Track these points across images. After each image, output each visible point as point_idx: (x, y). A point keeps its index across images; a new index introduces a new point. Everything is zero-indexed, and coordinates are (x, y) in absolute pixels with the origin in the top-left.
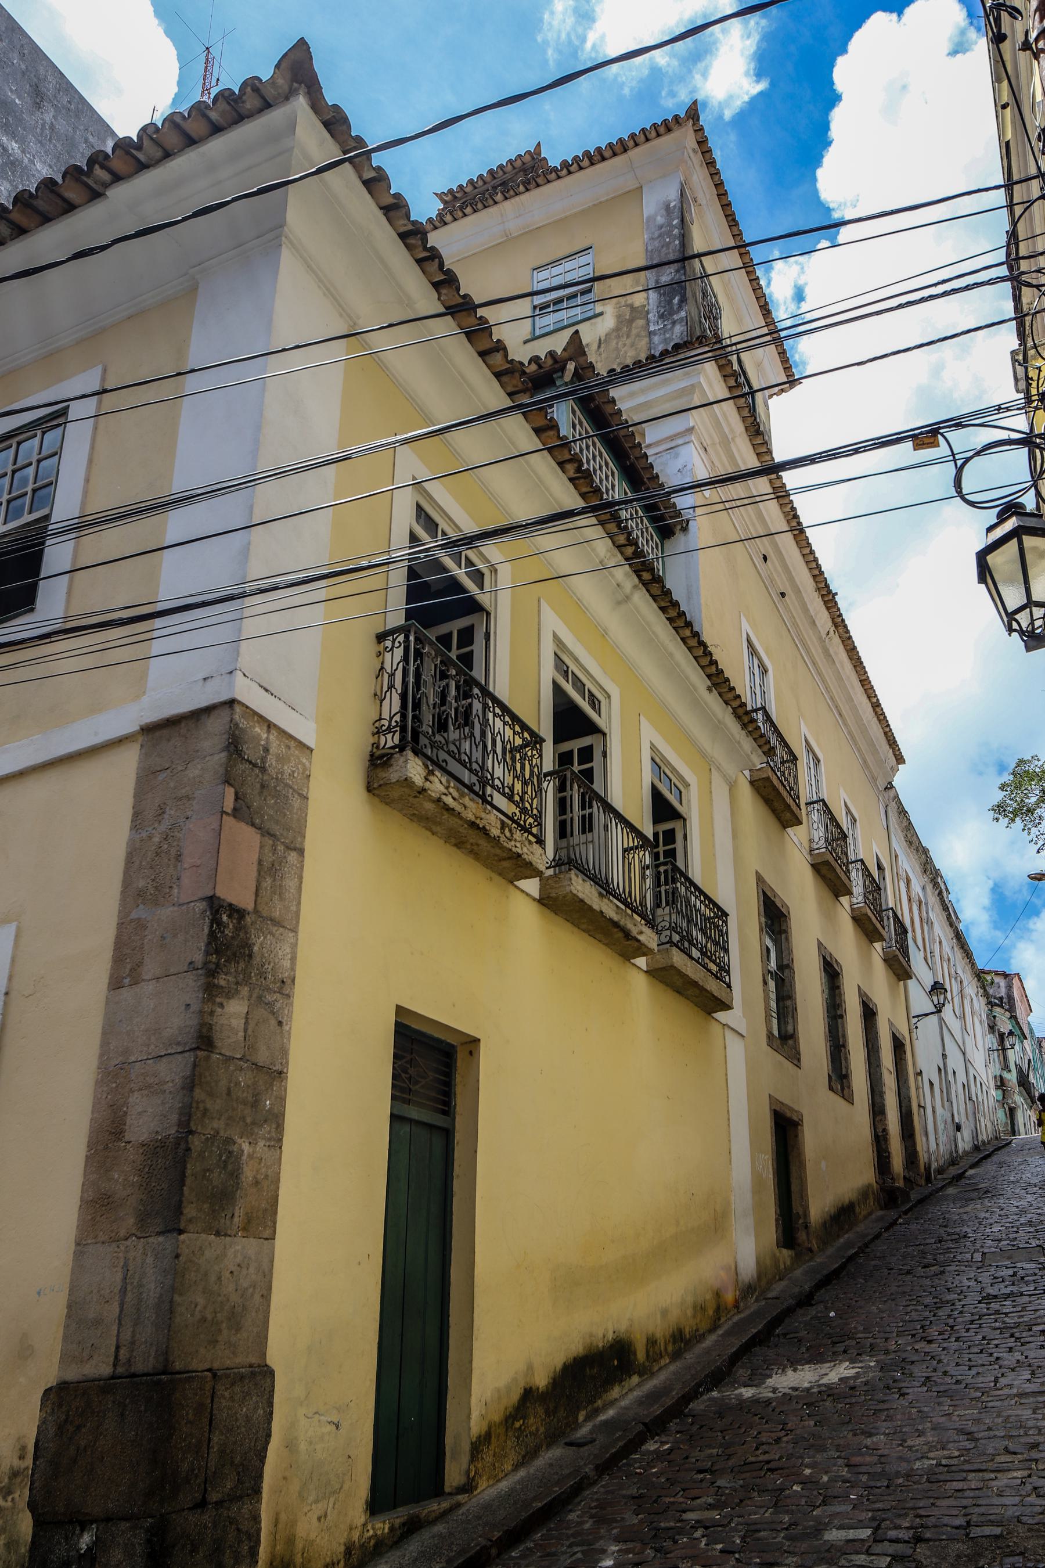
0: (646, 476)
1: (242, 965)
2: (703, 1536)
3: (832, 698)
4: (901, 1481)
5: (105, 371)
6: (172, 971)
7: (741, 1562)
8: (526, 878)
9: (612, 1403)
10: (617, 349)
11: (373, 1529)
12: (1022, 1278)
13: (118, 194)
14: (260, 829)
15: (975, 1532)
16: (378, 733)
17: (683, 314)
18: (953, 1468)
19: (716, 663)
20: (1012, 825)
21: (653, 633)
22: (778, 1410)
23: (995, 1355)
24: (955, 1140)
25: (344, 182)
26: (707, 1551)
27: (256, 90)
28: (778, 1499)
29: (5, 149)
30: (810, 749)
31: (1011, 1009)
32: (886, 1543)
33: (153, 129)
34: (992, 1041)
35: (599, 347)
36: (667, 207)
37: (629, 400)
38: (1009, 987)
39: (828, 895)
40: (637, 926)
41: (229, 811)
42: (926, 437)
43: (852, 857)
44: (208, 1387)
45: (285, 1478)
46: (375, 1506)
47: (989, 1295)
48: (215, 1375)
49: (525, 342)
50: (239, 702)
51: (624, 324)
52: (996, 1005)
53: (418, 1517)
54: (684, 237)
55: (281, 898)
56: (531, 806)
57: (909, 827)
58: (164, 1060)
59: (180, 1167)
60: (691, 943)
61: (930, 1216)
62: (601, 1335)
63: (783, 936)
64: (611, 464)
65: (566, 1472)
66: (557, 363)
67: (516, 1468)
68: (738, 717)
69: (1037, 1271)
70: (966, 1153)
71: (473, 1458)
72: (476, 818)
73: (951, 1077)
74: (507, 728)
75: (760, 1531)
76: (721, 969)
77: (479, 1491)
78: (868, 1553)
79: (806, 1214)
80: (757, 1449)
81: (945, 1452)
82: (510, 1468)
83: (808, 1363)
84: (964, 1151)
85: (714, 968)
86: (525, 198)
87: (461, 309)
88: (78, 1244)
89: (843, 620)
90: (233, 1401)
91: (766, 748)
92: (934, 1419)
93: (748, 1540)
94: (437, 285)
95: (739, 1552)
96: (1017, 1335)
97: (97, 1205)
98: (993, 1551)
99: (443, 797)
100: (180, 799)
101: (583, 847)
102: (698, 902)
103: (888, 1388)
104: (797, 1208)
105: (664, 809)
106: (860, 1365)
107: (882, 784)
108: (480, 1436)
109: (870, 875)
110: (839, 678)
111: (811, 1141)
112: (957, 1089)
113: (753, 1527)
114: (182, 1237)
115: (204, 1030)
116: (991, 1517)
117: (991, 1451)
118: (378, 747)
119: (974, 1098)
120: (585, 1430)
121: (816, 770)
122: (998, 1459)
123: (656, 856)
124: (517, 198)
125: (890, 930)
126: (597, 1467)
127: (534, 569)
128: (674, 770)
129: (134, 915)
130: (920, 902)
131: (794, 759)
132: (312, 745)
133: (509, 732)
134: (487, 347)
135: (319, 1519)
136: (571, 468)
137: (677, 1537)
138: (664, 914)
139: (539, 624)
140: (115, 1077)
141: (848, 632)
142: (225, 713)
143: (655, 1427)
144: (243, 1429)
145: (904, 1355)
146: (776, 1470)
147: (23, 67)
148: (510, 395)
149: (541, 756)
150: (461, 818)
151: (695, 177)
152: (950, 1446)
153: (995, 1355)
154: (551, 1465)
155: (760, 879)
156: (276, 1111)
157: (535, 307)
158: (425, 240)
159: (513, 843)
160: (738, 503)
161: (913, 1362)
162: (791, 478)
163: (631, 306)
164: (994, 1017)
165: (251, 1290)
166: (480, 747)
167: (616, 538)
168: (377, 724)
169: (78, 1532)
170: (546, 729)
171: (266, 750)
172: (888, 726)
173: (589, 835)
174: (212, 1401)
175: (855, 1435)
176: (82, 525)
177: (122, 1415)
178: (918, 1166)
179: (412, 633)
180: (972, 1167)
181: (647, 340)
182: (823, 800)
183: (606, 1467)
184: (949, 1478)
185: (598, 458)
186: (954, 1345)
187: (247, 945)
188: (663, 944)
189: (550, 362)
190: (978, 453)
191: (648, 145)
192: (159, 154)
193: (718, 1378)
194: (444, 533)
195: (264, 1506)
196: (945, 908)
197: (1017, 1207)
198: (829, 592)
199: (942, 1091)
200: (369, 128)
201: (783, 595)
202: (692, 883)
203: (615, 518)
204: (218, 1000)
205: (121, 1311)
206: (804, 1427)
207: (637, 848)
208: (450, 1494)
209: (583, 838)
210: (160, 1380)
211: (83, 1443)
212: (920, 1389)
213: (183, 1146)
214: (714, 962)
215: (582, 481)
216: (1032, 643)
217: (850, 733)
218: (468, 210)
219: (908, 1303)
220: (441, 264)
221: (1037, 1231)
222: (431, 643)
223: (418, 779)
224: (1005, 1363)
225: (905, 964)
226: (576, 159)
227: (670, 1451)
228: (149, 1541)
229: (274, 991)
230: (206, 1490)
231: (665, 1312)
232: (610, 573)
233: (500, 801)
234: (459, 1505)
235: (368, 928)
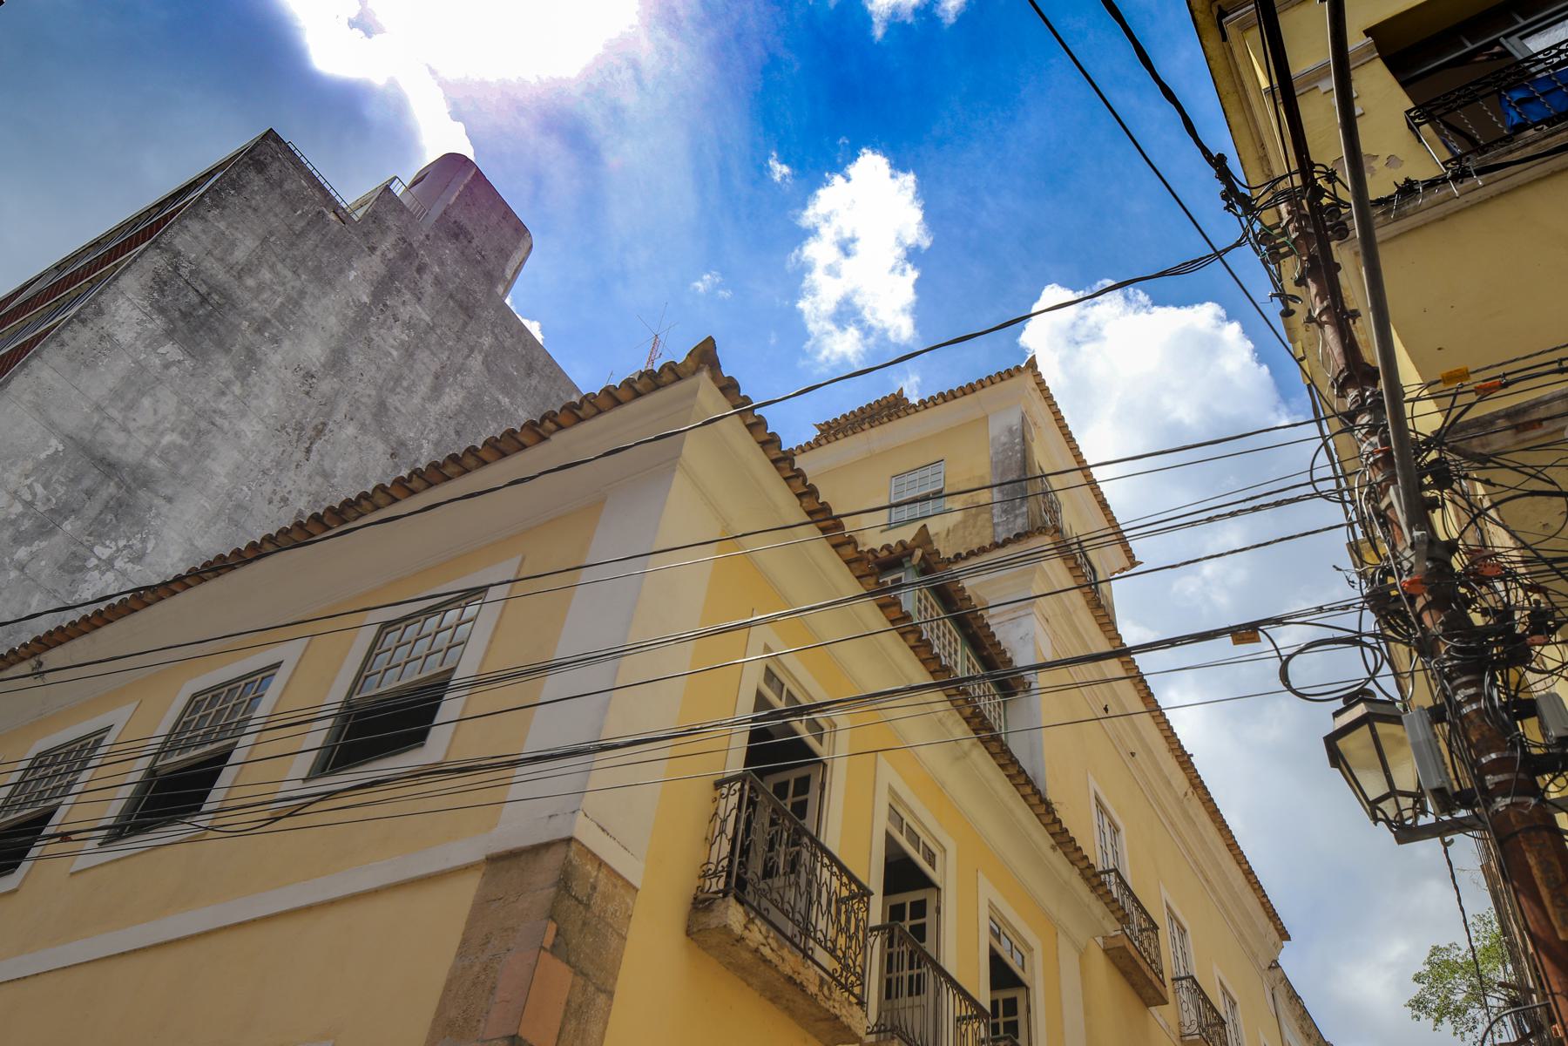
3: (1195, 862)
13: (558, 439)
19: (1060, 822)
25: (733, 430)
30: (1173, 917)
36: (1010, 430)
42: (1246, 632)
66: (906, 550)
68: (1087, 880)
87: (824, 518)
91: (1120, 913)
101: (908, 1012)
105: (1002, 975)
107: (1265, 964)
121: (1182, 941)
128: (1015, 932)
132: (638, 884)
133: (835, 883)
134: (843, 544)
136: (912, 638)
142: (561, 850)
149: (868, 910)
158: (792, 462)
170: (876, 883)
171: (594, 888)
173: (917, 999)
189: (900, 549)
190: (1300, 651)
192: (594, 411)
201: (1133, 754)
209: (909, 1001)
222: (765, 793)
226: (932, 398)
233: (821, 955)
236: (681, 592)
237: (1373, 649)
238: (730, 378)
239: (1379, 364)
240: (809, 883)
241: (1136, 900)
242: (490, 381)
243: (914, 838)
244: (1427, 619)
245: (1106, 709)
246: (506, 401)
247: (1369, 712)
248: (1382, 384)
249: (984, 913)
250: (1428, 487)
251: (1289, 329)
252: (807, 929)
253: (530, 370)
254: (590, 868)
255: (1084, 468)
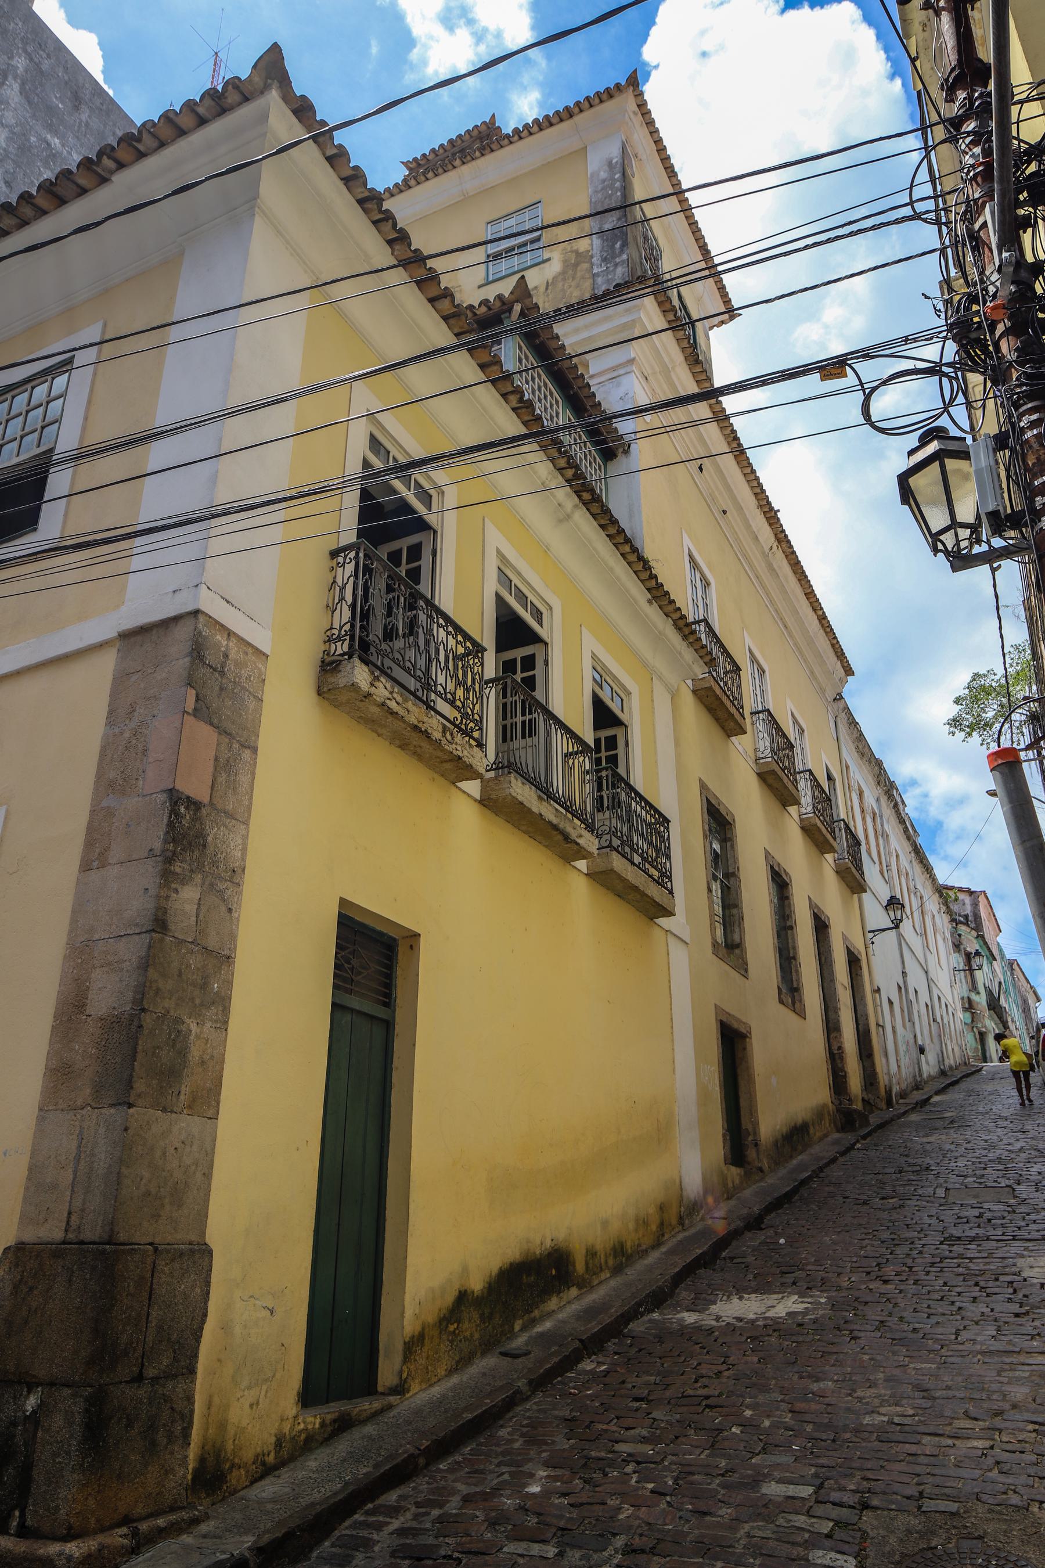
0: (588, 404)
1: (196, 854)
2: (634, 1472)
3: (776, 611)
4: (848, 1435)
5: (105, 325)
6: (135, 857)
7: (672, 1506)
8: (467, 779)
9: (550, 1314)
10: (563, 290)
11: (304, 1422)
12: (989, 1221)
13: (120, 179)
14: (217, 728)
15: (928, 1505)
16: (329, 641)
17: (625, 257)
18: (907, 1428)
19: (656, 577)
20: (969, 739)
21: (594, 548)
22: (720, 1341)
23: (957, 1304)
24: (919, 1063)
25: (309, 156)
26: (638, 1489)
27: (236, 87)
28: (715, 1441)
29: (49, 144)
30: (754, 660)
31: (978, 927)
32: (829, 1505)
33: (151, 124)
34: (957, 960)
35: (547, 289)
36: (610, 163)
37: (571, 335)
38: (975, 905)
39: (775, 805)
40: (575, 829)
41: (190, 711)
42: (833, 367)
43: (799, 767)
44: (149, 1260)
45: (219, 1360)
46: (307, 1398)
47: (952, 1236)
48: (156, 1250)
49: (479, 287)
50: (203, 613)
51: (570, 266)
52: (961, 923)
53: (349, 1414)
54: (626, 188)
55: (235, 793)
56: (472, 711)
57: (860, 737)
58: (123, 939)
59: (135, 1044)
60: (633, 850)
61: (890, 1143)
62: (538, 1242)
63: (729, 844)
64: (555, 394)
65: (499, 1383)
66: (505, 305)
67: (450, 1373)
68: (679, 629)
69: (1006, 1214)
70: (931, 1078)
71: (406, 1359)
72: (419, 722)
73: (912, 996)
74: (450, 637)
75: (693, 1474)
76: (663, 875)
77: (411, 1394)
78: (809, 1514)
79: (756, 1132)
80: (696, 1381)
81: (898, 1409)
82: (443, 1373)
83: (755, 1291)
84: (930, 1076)
85: (656, 874)
86: (481, 162)
87: (413, 261)
88: (41, 1110)
89: (786, 536)
90: (172, 1277)
92: (887, 1370)
93: (681, 1482)
94: (390, 242)
95: (671, 1495)
96: (982, 1284)
97: (60, 1074)
98: (947, 1531)
99: (388, 702)
100: (149, 699)
102: (639, 808)
103: (839, 1329)
104: (746, 1124)
105: (604, 716)
106: (810, 1300)
107: (830, 695)
108: (413, 1337)
109: (819, 786)
110: (784, 591)
111: (761, 1054)
112: (919, 1008)
113: (688, 1469)
114: (131, 1111)
115: (160, 914)
116: (946, 1490)
117: (948, 1413)
118: (328, 654)
119: (939, 1020)
120: (520, 1341)
121: (761, 680)
122: (958, 1424)
123: (598, 761)
124: (474, 163)
125: (842, 842)
126: (530, 1382)
127: (475, 491)
128: (615, 678)
129: (104, 804)
130: (874, 814)
131: (738, 669)
132: (267, 651)
133: (452, 642)
135: (251, 1406)
136: (514, 399)
137: (607, 1470)
138: (603, 819)
139: (484, 541)
140: (81, 952)
141: (791, 547)
143: (592, 1345)
144: (181, 1307)
145: (857, 1294)
146: (716, 1407)
147: (66, 78)
148: (457, 335)
149: (482, 664)
150: (404, 722)
151: (636, 136)
152: (904, 1402)
153: (957, 1304)
154: (484, 1374)
155: (703, 787)
156: (223, 994)
157: (488, 256)
159: (454, 746)
160: (675, 428)
161: (866, 1303)
162: (730, 403)
163: (577, 252)
164: (960, 935)
165: (193, 1168)
166: (424, 656)
167: (557, 461)
168: (328, 633)
169: (25, 1393)
170: (488, 639)
171: (226, 656)
172: (835, 638)
173: (529, 741)
174: (152, 1275)
175: (801, 1378)
176: (81, 456)
177: (70, 1280)
178: (878, 1089)
179: (362, 550)
180: (937, 1093)
181: (591, 281)
182: (768, 711)
183: (540, 1383)
184: (901, 1439)
185: (543, 389)
186: (911, 1288)
187: (202, 835)
188: (604, 848)
189: (498, 304)
191: (593, 110)
192: (156, 144)
193: (658, 1299)
194: (395, 459)
195: (198, 1386)
196: (902, 821)
197: (986, 1141)
198: (772, 509)
199: (902, 1010)
200: (327, 112)
201: (724, 512)
202: (632, 789)
203: (557, 443)
204: (173, 886)
205: (75, 1178)
206: (746, 1363)
207: (576, 753)
208: (383, 1394)
209: (523, 742)
210: (105, 1250)
211: (34, 1304)
212: (873, 1334)
213: (136, 1023)
214: (656, 868)
215: (524, 410)
216: (957, 563)
217: (796, 644)
218: (430, 175)
219: (863, 1236)
220: (395, 224)
221: (1006, 1169)
223: (364, 686)
224: (969, 1314)
225: (858, 877)
227: (607, 1373)
228: (87, 1411)
229: (225, 880)
230: (143, 1365)
231: (605, 1224)
232: (552, 494)
233: (442, 706)
234: (390, 1407)
235: (319, 823)
236: (276, 350)
237: (950, 378)
238: (303, 97)
239: (992, 62)
240: (427, 643)
241: (722, 646)
242: (34, 116)
243: (522, 598)
244: (1004, 346)
245: (701, 469)
246: (56, 142)
247: (939, 446)
248: (992, 86)
249: (588, 663)
250: (1025, 203)
251: (904, 21)
252: (428, 684)
253: (77, 102)
254: (220, 638)
255: (679, 193)
